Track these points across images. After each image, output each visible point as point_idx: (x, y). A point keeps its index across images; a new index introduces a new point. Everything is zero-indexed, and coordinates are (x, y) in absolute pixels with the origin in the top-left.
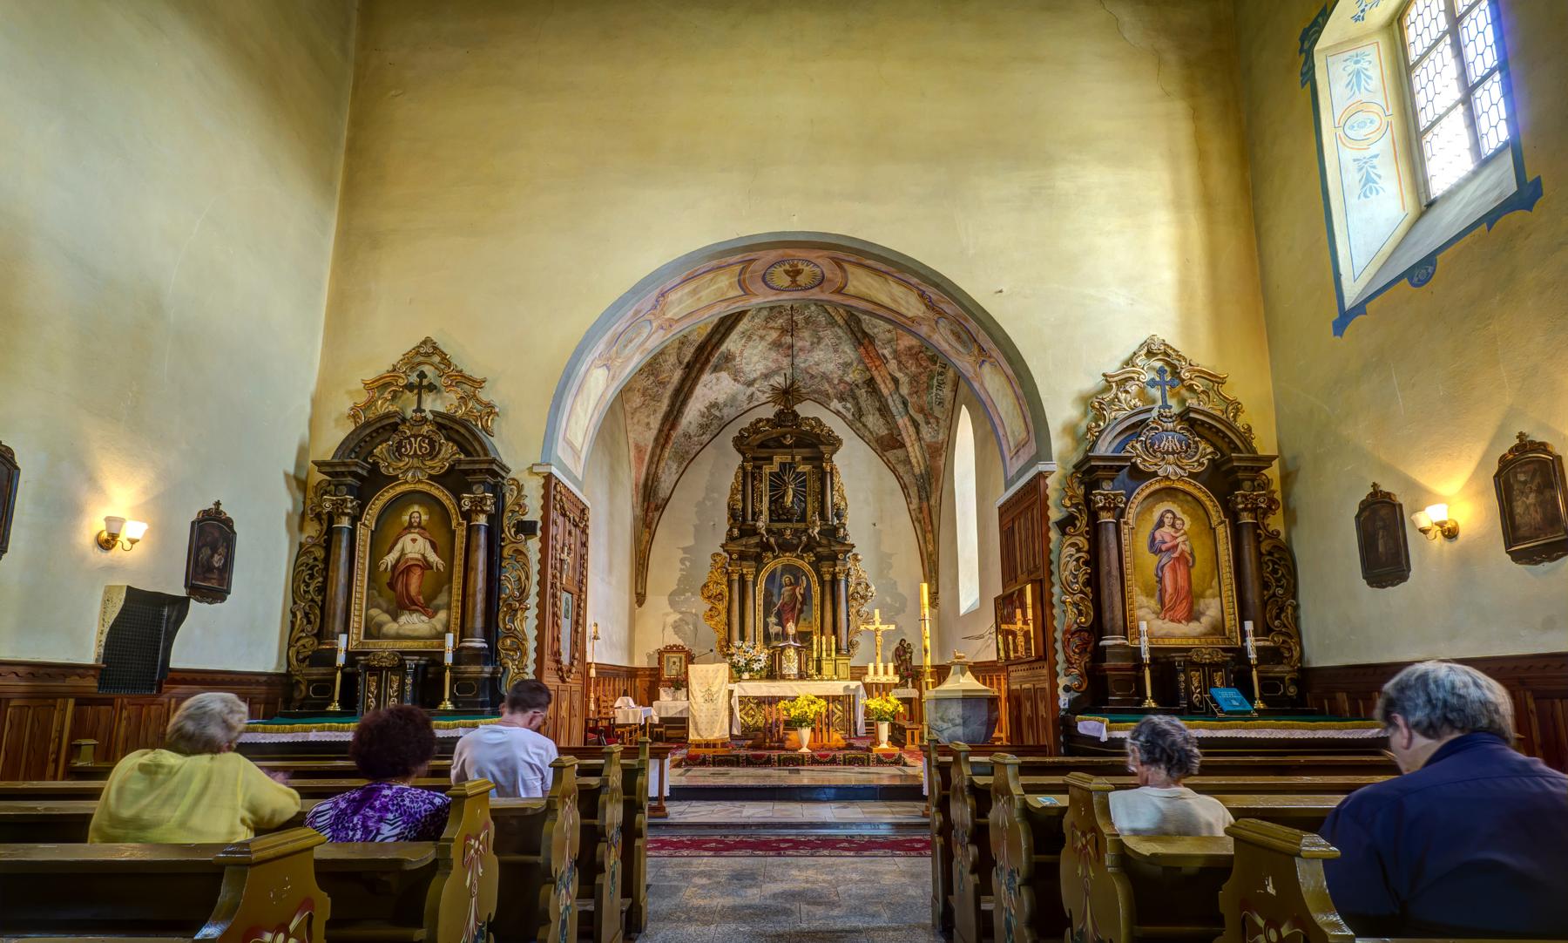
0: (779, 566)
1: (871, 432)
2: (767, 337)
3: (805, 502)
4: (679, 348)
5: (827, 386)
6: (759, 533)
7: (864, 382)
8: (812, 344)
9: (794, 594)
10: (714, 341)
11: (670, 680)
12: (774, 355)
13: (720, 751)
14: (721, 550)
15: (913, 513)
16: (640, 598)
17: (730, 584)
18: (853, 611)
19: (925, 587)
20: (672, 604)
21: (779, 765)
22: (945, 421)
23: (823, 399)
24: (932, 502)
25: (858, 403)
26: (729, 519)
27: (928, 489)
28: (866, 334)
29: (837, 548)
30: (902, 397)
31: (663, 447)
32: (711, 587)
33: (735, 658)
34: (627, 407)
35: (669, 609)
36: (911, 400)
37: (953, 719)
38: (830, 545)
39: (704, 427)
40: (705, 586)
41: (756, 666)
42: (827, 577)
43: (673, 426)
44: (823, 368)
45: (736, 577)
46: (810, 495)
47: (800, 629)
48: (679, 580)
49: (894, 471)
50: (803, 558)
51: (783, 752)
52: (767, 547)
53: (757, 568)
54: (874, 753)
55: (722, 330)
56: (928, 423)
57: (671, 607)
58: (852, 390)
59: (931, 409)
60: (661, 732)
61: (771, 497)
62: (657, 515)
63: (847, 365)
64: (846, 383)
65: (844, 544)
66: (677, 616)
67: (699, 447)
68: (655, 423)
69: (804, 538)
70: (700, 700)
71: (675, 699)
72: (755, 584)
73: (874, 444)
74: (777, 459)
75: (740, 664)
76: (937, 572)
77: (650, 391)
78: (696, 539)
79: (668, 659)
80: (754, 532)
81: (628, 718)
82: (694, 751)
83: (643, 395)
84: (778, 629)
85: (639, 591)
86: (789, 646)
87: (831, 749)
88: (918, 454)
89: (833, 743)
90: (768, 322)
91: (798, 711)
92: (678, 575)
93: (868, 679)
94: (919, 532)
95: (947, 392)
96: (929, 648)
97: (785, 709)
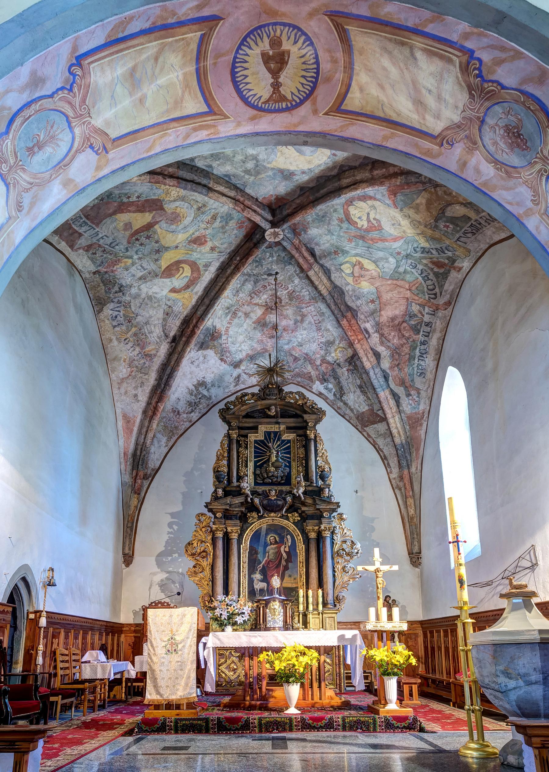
0: (264, 526)
1: (352, 410)
2: (252, 315)
3: (290, 467)
4: (164, 320)
5: (309, 368)
6: (244, 494)
7: (346, 360)
8: (296, 322)
10: (199, 313)
12: (258, 335)
13: (185, 713)
14: (205, 511)
15: (393, 482)
16: (128, 559)
18: (339, 567)
20: (159, 564)
21: (260, 731)
23: (306, 382)
24: (413, 470)
25: (339, 383)
26: (214, 482)
27: (409, 458)
28: (349, 308)
29: (322, 506)
30: (383, 371)
31: (151, 418)
32: (195, 545)
33: (217, 612)
34: (113, 376)
37: (526, 675)
38: (315, 504)
39: (192, 405)
41: (239, 619)
42: (313, 535)
43: (160, 399)
45: (220, 535)
46: (294, 460)
47: (285, 585)
48: (167, 542)
49: (374, 445)
50: (287, 518)
51: (266, 714)
52: (252, 508)
53: (242, 528)
54: (382, 715)
55: (207, 301)
56: (408, 395)
57: (158, 567)
58: (333, 370)
61: (255, 462)
62: (146, 483)
63: (330, 343)
64: (328, 363)
65: (330, 503)
66: (164, 576)
67: (187, 424)
68: (143, 398)
69: (289, 499)
70: (161, 651)
72: (239, 543)
73: (354, 421)
74: (262, 428)
75: (223, 617)
77: (136, 362)
78: (184, 503)
80: (239, 492)
81: (96, 673)
82: (151, 714)
83: (130, 366)
84: (264, 585)
85: (127, 551)
86: (274, 600)
87: (323, 709)
88: (399, 425)
89: (325, 701)
90: (252, 298)
91: (284, 664)
92: (166, 537)
93: (370, 626)
94: (399, 498)
95: (429, 362)
96: (465, 578)
97: (268, 662)
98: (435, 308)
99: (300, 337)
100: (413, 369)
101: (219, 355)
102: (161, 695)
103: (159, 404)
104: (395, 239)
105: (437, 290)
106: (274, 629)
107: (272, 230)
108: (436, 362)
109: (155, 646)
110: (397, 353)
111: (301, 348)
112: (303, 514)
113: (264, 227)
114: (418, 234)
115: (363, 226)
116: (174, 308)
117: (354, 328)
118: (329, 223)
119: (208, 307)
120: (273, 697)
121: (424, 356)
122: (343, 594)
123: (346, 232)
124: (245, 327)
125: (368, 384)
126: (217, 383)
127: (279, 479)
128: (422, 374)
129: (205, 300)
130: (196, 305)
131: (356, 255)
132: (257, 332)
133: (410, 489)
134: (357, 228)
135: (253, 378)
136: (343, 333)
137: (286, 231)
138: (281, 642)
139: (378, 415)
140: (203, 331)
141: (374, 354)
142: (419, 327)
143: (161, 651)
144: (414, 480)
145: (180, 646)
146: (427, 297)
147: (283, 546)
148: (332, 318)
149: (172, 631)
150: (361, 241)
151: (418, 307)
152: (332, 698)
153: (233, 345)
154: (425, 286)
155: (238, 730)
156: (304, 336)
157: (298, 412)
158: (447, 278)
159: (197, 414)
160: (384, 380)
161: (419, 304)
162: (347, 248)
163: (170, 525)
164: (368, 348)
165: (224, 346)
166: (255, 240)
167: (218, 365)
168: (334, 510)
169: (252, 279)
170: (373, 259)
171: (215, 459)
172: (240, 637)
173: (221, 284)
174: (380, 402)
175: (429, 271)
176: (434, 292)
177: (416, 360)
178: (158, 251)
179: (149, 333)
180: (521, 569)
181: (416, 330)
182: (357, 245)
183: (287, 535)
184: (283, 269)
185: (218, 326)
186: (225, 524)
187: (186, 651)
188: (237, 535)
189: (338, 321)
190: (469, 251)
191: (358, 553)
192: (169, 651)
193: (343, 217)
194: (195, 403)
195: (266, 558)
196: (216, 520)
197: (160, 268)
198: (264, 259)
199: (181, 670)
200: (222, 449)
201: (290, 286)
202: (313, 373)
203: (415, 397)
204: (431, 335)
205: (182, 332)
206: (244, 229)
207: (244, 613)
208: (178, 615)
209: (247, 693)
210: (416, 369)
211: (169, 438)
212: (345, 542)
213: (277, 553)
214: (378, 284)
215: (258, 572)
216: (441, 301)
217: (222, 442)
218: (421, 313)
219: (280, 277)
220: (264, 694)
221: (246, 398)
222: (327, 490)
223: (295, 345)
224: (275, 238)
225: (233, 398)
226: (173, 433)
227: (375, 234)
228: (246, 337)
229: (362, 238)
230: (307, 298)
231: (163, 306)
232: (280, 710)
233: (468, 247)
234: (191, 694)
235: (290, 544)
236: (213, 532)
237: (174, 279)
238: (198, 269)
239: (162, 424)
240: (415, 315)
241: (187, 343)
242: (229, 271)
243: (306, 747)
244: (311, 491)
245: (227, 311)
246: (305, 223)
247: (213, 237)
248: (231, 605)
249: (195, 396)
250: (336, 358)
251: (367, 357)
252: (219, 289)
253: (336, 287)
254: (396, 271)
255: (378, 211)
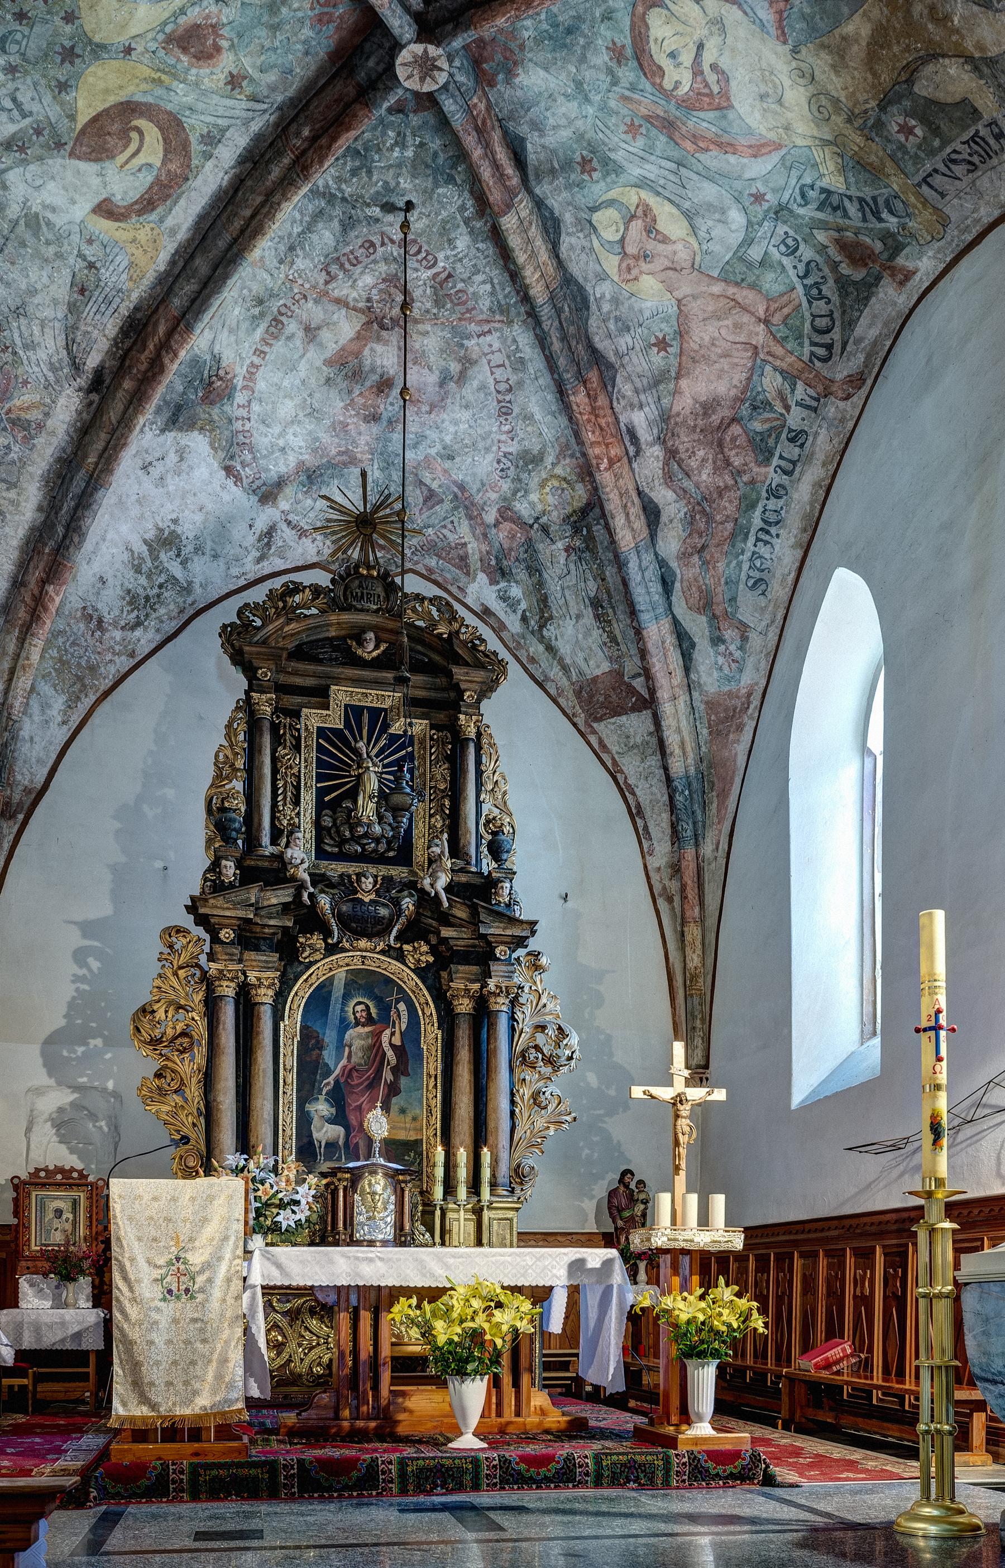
0: (341, 976)
1: (565, 668)
2: (325, 335)
4: (73, 308)
5: (464, 531)
6: (293, 879)
9: (377, 1045)
10: (177, 303)
11: (44, 1255)
12: (336, 405)
13: (214, 1449)
14: (187, 921)
15: (655, 877)
17: (212, 1005)
18: (526, 1092)
19: (679, 1048)
20: (52, 1064)
21: (404, 1492)
22: (764, 634)
24: (707, 849)
25: (540, 584)
26: (209, 841)
28: (596, 357)
29: (493, 929)
30: (662, 563)
32: (160, 1014)
35: (42, 1078)
36: (684, 573)
38: (475, 921)
40: (145, 1011)
42: (464, 1006)
44: (463, 470)
45: (228, 990)
48: (71, 1005)
49: (614, 773)
50: (400, 957)
53: (284, 974)
54: (682, 1449)
55: (202, 265)
56: (717, 640)
57: (50, 1075)
58: (529, 545)
59: (733, 599)
60: (23, 1388)
61: (321, 793)
63: (529, 460)
64: (517, 520)
65: (513, 921)
66: (65, 1097)
67: (124, 663)
69: (408, 903)
70: (149, 1291)
71: (60, 1304)
72: (278, 1016)
74: (341, 695)
76: (708, 1020)
79: (42, 1207)
82: (125, 1452)
84: (334, 1132)
88: (684, 723)
89: (531, 1420)
90: (331, 278)
92: (67, 991)
98: (820, 388)
99: (452, 429)
100: (739, 565)
101: (222, 454)
102: (153, 1407)
103: (50, 589)
104: (758, 150)
105: (836, 335)
106: (371, 1243)
107: (418, 48)
108: (799, 553)
109: (132, 1277)
110: (703, 511)
111: (448, 464)
112: (443, 948)
113: (396, 32)
114: (825, 143)
115: (677, 84)
116: (104, 274)
117: (603, 422)
118: (583, 59)
119: (205, 285)
120: (405, 1410)
121: (773, 530)
122: (531, 1162)
123: (625, 98)
124: (303, 374)
125: (617, 597)
126: (209, 545)
127: (382, 847)
128: (759, 584)
129: (197, 261)
130: (167, 273)
131: (642, 183)
132: (333, 393)
133: (696, 901)
134: (660, 88)
135: (307, 542)
136: (568, 432)
137: (457, 63)
138: (432, 1275)
139: (632, 691)
140: (185, 369)
141: (644, 509)
142: (771, 442)
143: (149, 1291)
144: (707, 877)
145: (200, 1280)
146: (807, 349)
147: (388, 1032)
148: (545, 380)
149: (177, 1239)
150: (663, 139)
151: (780, 379)
152: (543, 1412)
153: (262, 427)
154: (807, 315)
155: (351, 1489)
156: (463, 427)
157: (437, 658)
158: (867, 299)
159: (151, 634)
160: (660, 589)
161: (782, 372)
162: (618, 156)
163: (80, 956)
164: (631, 487)
165: (238, 425)
166: (361, 76)
167: (216, 485)
168: (520, 942)
169: (338, 211)
170: (687, 205)
171: (211, 771)
172: (331, 1262)
173: (248, 213)
174: (643, 654)
175: (826, 271)
176: (826, 339)
177: (752, 539)
178: (69, 55)
179: (26, 347)
180: (989, 1111)
181: (764, 452)
182: (649, 150)
183: (398, 1002)
184: (428, 194)
185: (228, 357)
186: (240, 961)
187: (217, 1293)
188: (271, 992)
189: (561, 392)
190: (944, 222)
191: (570, 1058)
192: (170, 1292)
193: (628, 42)
194: (147, 598)
195: (344, 1062)
196: (218, 948)
197: (72, 118)
198: (379, 150)
199: (204, 1341)
200: (231, 745)
201: (441, 256)
202: (474, 548)
203: (732, 648)
204: (798, 469)
205: (123, 359)
206: (332, 26)
207: (297, 1203)
208: (193, 1199)
209: (342, 1402)
210: (745, 566)
211: (73, 700)
212: (542, 1028)
213: (371, 1048)
214: (685, 290)
215: (322, 1098)
216: (841, 370)
217: (229, 726)
218: (783, 399)
219: (418, 223)
220: (384, 1402)
221: (297, 598)
222: (508, 885)
223: (433, 451)
224: (422, 80)
225: (258, 595)
226: (84, 686)
227: (703, 122)
228: (303, 405)
229: (668, 126)
230: (485, 304)
231: (71, 260)
232: (438, 1442)
233: (947, 210)
234: (231, 1402)
235: (404, 1027)
236: (208, 981)
237: (111, 168)
238: (185, 145)
239: (55, 653)
240: (767, 405)
241: (138, 398)
242: (276, 172)
243: (543, 1525)
244: (467, 886)
245: (256, 311)
246: (513, 45)
247: (240, 36)
248: (262, 1182)
249: (149, 577)
250: (540, 507)
251: (627, 515)
252: (242, 231)
253: (568, 280)
254: (740, 257)
255: (729, 40)
